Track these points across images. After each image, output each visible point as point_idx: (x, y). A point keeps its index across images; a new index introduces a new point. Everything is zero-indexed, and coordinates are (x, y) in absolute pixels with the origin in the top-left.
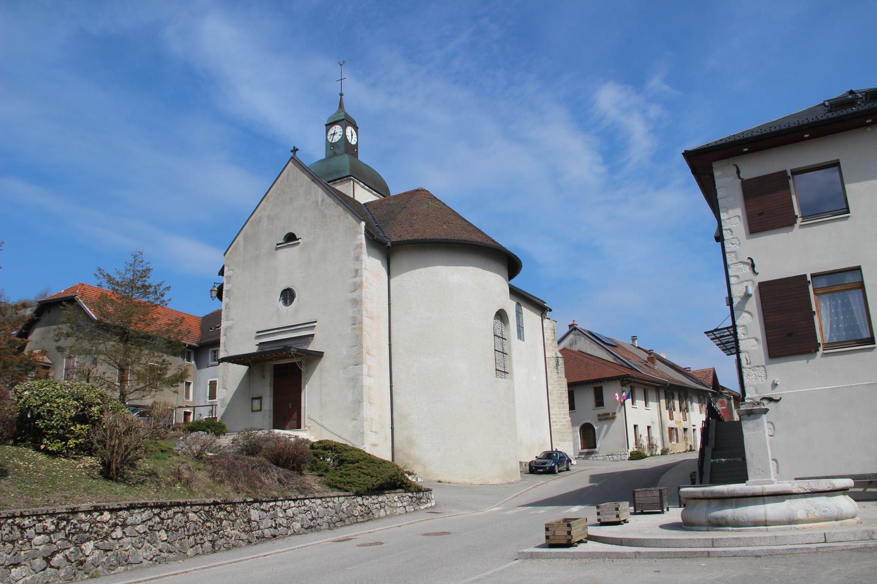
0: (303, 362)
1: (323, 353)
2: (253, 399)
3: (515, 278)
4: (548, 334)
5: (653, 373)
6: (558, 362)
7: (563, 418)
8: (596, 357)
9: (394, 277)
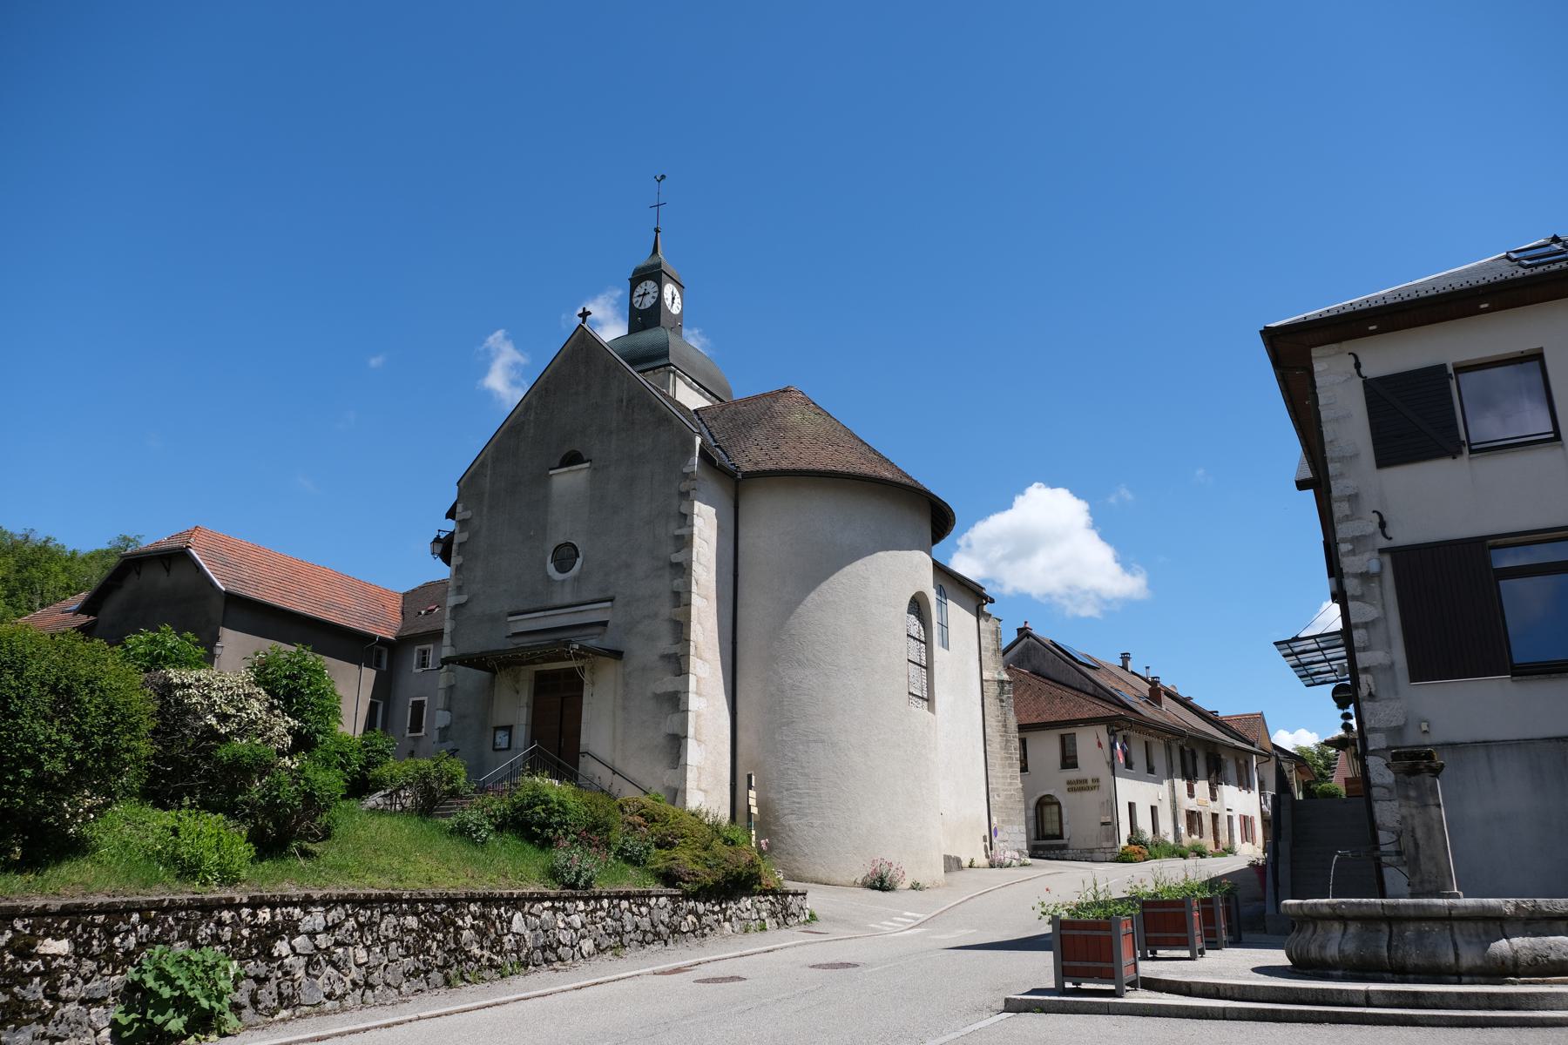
0: (587, 667)
3: (942, 542)
4: (987, 641)
7: (1010, 784)
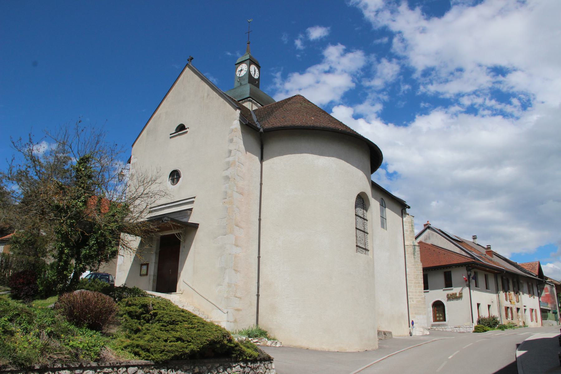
1: (198, 224)
2: (142, 265)
5: (491, 263)
6: (414, 249)
7: (419, 295)
8: (445, 249)
9: (266, 160)
